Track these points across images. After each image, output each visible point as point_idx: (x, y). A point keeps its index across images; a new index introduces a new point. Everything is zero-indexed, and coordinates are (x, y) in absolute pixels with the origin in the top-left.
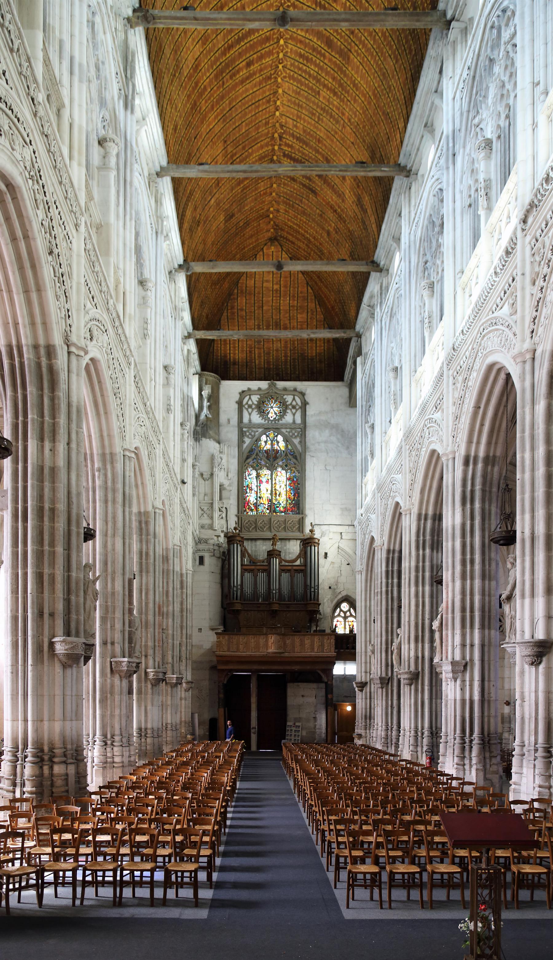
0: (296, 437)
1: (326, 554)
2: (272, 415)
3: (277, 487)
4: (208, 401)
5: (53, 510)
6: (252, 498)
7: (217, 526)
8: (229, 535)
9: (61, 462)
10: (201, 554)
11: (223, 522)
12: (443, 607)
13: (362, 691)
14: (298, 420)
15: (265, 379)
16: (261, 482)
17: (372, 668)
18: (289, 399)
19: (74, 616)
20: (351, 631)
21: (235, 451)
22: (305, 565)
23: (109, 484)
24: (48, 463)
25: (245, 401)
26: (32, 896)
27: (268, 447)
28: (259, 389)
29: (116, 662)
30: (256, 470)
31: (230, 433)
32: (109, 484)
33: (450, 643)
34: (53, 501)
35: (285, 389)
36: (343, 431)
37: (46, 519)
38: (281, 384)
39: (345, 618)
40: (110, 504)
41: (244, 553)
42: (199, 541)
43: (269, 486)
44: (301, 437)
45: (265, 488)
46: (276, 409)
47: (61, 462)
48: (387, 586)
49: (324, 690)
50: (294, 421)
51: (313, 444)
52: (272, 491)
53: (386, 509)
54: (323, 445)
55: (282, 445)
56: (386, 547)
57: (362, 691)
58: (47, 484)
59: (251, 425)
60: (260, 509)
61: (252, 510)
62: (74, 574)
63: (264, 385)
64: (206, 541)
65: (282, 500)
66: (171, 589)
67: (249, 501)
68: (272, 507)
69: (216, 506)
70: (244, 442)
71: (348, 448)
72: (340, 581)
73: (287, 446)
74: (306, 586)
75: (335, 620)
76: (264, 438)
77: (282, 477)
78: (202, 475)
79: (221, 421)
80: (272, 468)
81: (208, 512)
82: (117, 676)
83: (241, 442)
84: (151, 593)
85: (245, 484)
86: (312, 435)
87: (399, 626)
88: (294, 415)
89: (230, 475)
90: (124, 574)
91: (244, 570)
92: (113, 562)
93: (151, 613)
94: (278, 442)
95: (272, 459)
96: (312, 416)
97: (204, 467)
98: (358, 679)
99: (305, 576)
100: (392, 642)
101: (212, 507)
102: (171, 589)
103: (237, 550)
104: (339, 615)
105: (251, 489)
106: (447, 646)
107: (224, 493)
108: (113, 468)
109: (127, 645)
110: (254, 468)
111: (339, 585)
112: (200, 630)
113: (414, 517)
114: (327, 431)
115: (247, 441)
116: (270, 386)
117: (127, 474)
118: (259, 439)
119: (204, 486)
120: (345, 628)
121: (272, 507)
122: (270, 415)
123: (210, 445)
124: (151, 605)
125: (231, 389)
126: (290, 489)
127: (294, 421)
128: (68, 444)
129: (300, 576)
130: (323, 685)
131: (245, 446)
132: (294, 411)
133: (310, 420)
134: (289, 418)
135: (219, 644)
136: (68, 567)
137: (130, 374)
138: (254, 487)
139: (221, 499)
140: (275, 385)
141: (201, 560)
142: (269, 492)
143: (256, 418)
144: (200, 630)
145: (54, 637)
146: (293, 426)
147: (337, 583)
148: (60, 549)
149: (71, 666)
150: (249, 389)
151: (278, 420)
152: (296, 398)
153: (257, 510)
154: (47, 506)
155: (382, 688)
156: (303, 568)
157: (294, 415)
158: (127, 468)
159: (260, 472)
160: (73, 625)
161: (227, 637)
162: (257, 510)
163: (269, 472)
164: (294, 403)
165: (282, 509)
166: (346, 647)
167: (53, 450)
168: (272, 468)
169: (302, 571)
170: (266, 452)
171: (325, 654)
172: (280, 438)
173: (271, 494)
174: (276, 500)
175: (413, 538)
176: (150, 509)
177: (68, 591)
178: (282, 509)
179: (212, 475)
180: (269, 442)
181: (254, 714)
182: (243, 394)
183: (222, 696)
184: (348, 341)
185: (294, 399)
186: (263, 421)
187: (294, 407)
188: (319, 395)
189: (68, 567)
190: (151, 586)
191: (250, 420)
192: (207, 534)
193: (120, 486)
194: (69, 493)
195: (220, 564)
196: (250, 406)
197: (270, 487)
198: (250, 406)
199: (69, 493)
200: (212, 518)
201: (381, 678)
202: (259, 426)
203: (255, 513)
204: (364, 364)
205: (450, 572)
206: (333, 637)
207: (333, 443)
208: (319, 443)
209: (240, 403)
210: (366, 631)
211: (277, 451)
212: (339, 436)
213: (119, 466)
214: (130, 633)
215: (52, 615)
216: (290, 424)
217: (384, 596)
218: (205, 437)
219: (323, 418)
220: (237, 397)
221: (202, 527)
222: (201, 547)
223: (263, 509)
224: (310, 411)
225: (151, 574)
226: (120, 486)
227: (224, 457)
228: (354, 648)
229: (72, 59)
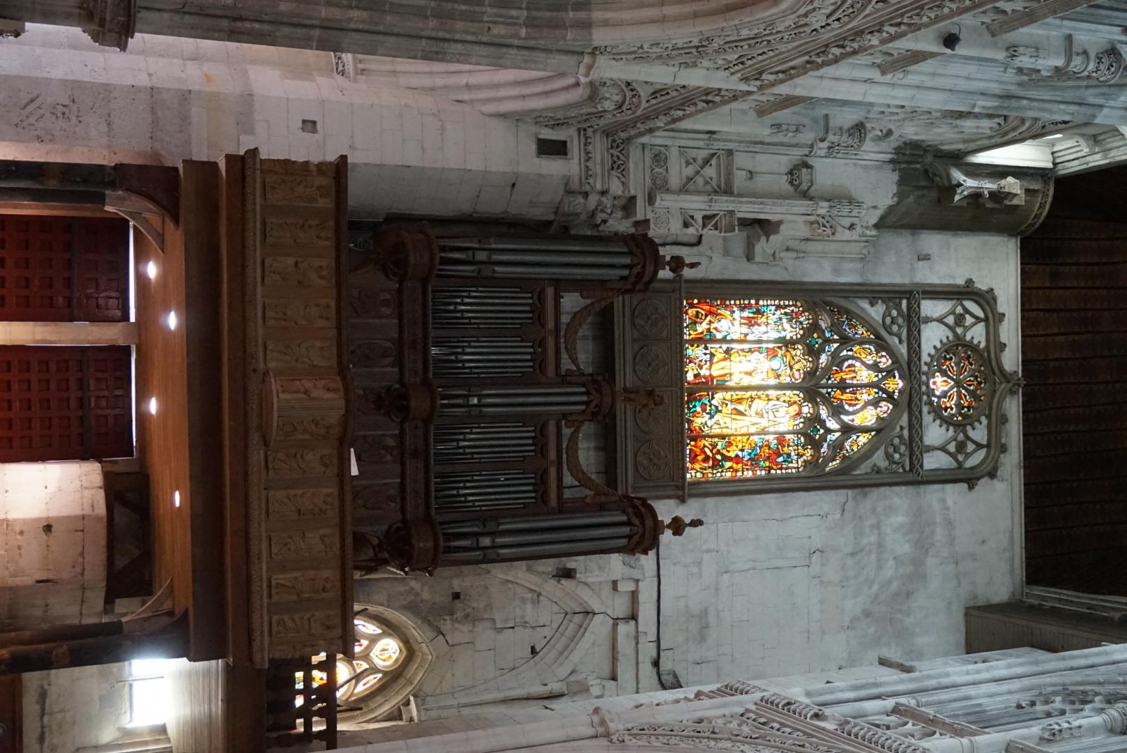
0: (888, 457)
3: (759, 405)
4: (994, 195)
6: (730, 323)
10: (575, 148)
15: (1025, 362)
16: (772, 354)
18: (979, 433)
21: (849, 277)
22: (563, 508)
25: (969, 305)
26: (345, 720)
31: (898, 264)
35: (1004, 420)
36: (909, 594)
38: (1013, 408)
50: (930, 449)
51: (874, 510)
54: (873, 539)
59: (914, 322)
63: (1011, 360)
68: (709, 386)
71: (867, 614)
72: (480, 627)
74: (489, 518)
77: (779, 417)
83: (875, 293)
96: (943, 501)
99: (525, 511)
105: (750, 323)
111: (465, 628)
114: (907, 548)
127: (930, 449)
129: (524, 491)
131: (865, 304)
138: (757, 332)
140: (1012, 392)
142: (746, 381)
143: (933, 337)
146: (915, 446)
147: (472, 618)
151: (930, 403)
152: (982, 454)
156: (553, 502)
157: (943, 449)
169: (543, 497)
174: (724, 403)
179: (805, 195)
182: (986, 299)
185: (979, 446)
186: (925, 358)
191: (928, 320)
196: (960, 320)
198: (960, 320)
200: (683, 190)
207: (880, 567)
208: (877, 526)
212: (895, 585)
218: (900, 183)
219: (940, 534)
220: (982, 285)
224: (953, 494)
229: (1101, 106)
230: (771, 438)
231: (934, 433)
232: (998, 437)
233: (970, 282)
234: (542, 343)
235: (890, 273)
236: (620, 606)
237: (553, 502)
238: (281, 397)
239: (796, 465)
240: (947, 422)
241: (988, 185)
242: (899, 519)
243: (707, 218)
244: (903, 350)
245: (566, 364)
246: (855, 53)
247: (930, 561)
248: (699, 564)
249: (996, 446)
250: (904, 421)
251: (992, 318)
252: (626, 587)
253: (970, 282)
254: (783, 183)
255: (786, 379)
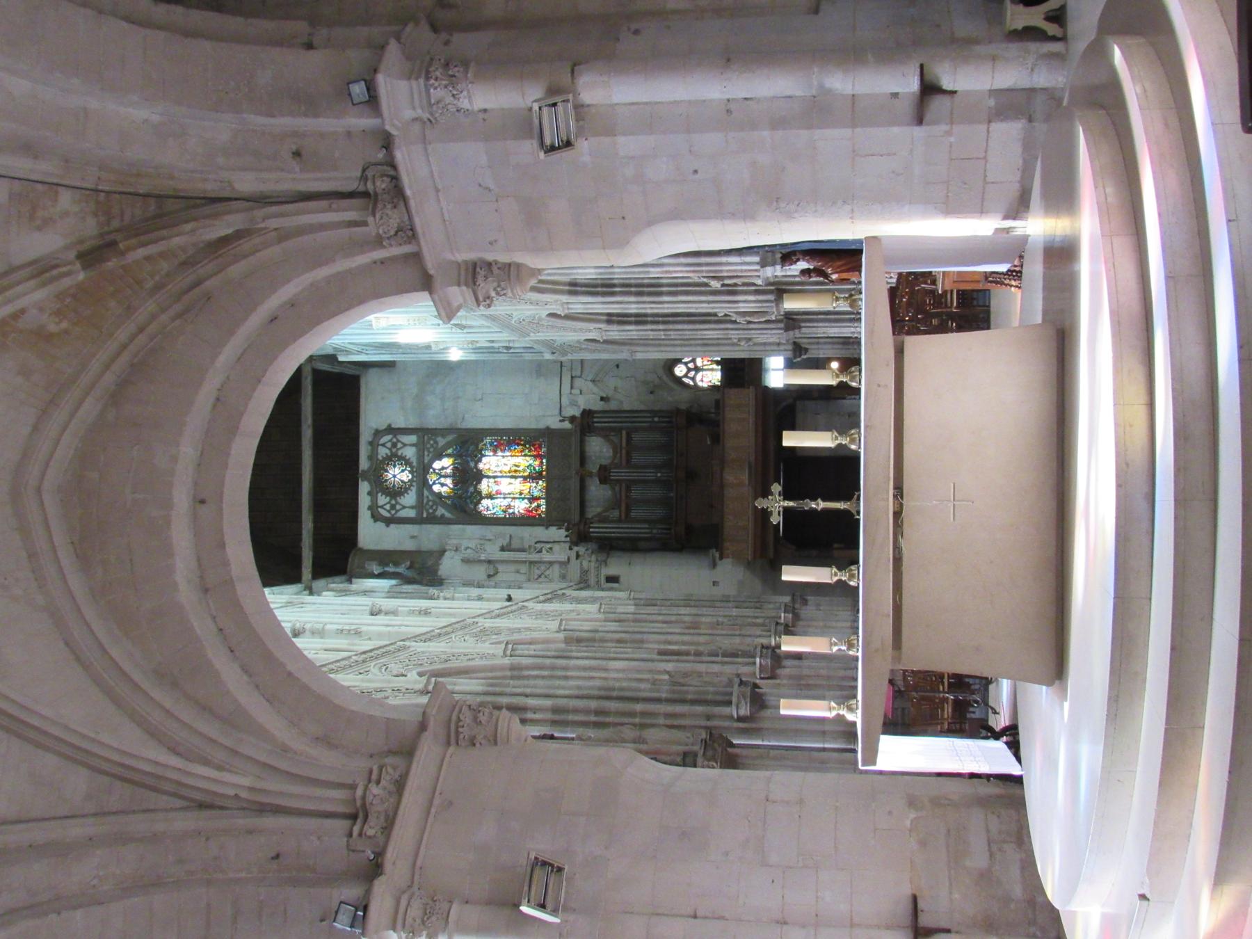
0: (436, 443)
1: (602, 399)
2: (406, 476)
3: (506, 469)
4: (387, 565)
5: (598, 712)
6: (520, 507)
7: (563, 558)
8: (575, 539)
9: (548, 703)
10: (603, 580)
11: (556, 547)
12: (695, 278)
13: (806, 350)
14: (413, 439)
17: (771, 340)
18: (383, 452)
19: (710, 697)
20: (718, 363)
23: (546, 673)
24: (549, 716)
25: (388, 515)
27: (449, 481)
28: (369, 493)
29: (761, 672)
30: (482, 498)
31: (430, 536)
32: (546, 673)
33: (739, 268)
34: (587, 711)
35: (370, 458)
37: (608, 720)
38: (364, 464)
39: (697, 369)
40: (569, 673)
41: (602, 519)
42: (584, 584)
43: (505, 481)
44: (436, 435)
45: (506, 486)
46: (397, 470)
47: (548, 703)
48: (658, 323)
49: (807, 402)
52: (512, 477)
53: (553, 327)
55: (447, 462)
56: (603, 326)
57: (806, 350)
58: (571, 717)
59: (420, 505)
60: (536, 494)
61: (539, 506)
62: (664, 695)
63: (364, 488)
64: (584, 572)
65: (524, 462)
66: (660, 618)
67: (527, 510)
68: (534, 477)
69: (534, 557)
70: (443, 516)
73: (449, 456)
75: (700, 384)
76: (436, 488)
77: (491, 462)
78: (489, 576)
79: (413, 548)
80: (479, 476)
81: (543, 568)
82: (779, 671)
83: (442, 521)
84: (669, 637)
85: (501, 515)
86: (434, 417)
87: (715, 315)
88: (405, 445)
89: (489, 536)
90: (652, 661)
91: (627, 518)
92: (638, 671)
93: (696, 639)
94: (443, 468)
95: (468, 477)
97: (480, 572)
98: (790, 354)
99: (636, 430)
100: (735, 322)
101: (536, 562)
102: (660, 618)
103: (596, 529)
104: (693, 379)
105: (509, 507)
106: (741, 271)
107: (515, 545)
108: (528, 668)
109: (740, 660)
110: (479, 502)
112: (715, 583)
113: (573, 299)
114: (429, 398)
115: (441, 511)
116: (365, 479)
117: (532, 653)
118: (439, 495)
119: (506, 573)
120: (712, 370)
121: (534, 477)
122: (406, 479)
123: (449, 565)
124: (686, 638)
125: (370, 534)
126: (510, 450)
128: (527, 696)
129: (636, 437)
130: (799, 404)
131: (448, 515)
132: (399, 445)
133: (412, 423)
134: (410, 453)
135: (738, 557)
136: (658, 700)
137: (420, 647)
138: (505, 502)
139: (523, 550)
141: (612, 579)
142: (513, 480)
143: (410, 499)
144: (715, 583)
145: (732, 717)
146: (421, 447)
147: (645, 383)
148: (639, 707)
149: (763, 701)
150: (370, 508)
151: (411, 467)
152: (382, 441)
153: (539, 498)
154: (593, 718)
155: (800, 327)
156: (624, 433)
157: (405, 445)
158: (526, 652)
159: (484, 492)
160: (719, 698)
161: (727, 544)
162: (539, 498)
163: (485, 481)
164: (389, 445)
165: (537, 463)
166: (742, 372)
167: (535, 710)
168: (479, 476)
170: (455, 484)
171: (752, 402)
172: (437, 465)
173: (516, 477)
174: (524, 471)
175: (600, 299)
176: (561, 636)
177: (683, 701)
178: (537, 463)
179: (489, 562)
180: (442, 480)
181: (821, 505)
182: (376, 517)
183: (814, 553)
184: (316, 373)
185: (383, 445)
186: (414, 489)
187: (394, 445)
188: (378, 410)
189: (658, 700)
190: (662, 637)
191: (412, 507)
192: (574, 570)
193: (548, 661)
194: (577, 697)
195: (619, 553)
196: (393, 507)
197: (509, 482)
199: (577, 697)
200: (551, 563)
201: (787, 329)
202: (420, 495)
203: (543, 502)
204: (348, 352)
205: (652, 269)
206: (726, 390)
208: (444, 410)
209: (389, 521)
210: (718, 345)
211: (455, 469)
213: (525, 661)
214: (724, 655)
215: (708, 718)
216: (419, 450)
217: (671, 327)
218: (436, 571)
219: (409, 404)
220: (380, 525)
221: (563, 577)
222: (592, 581)
223: (538, 488)
224: (400, 423)
225: (645, 636)
226: (548, 661)
227: (465, 543)
228: (742, 360)
230: (500, 453)
231: (410, 453)
232: (372, 450)
233: (388, 526)
234: (627, 497)
235: (434, 531)
236: (578, 382)
237: (624, 433)
238: (745, 477)
239: (488, 440)
240: (401, 458)
241: (391, 569)
242: (431, 412)
243: (540, 551)
244: (426, 493)
245: (617, 488)
246: (364, 653)
247: (415, 391)
248: (540, 399)
249: (374, 444)
250: (427, 460)
251: (373, 508)
252: (576, 391)
253: (388, 526)
254: (501, 568)
255: (492, 480)
